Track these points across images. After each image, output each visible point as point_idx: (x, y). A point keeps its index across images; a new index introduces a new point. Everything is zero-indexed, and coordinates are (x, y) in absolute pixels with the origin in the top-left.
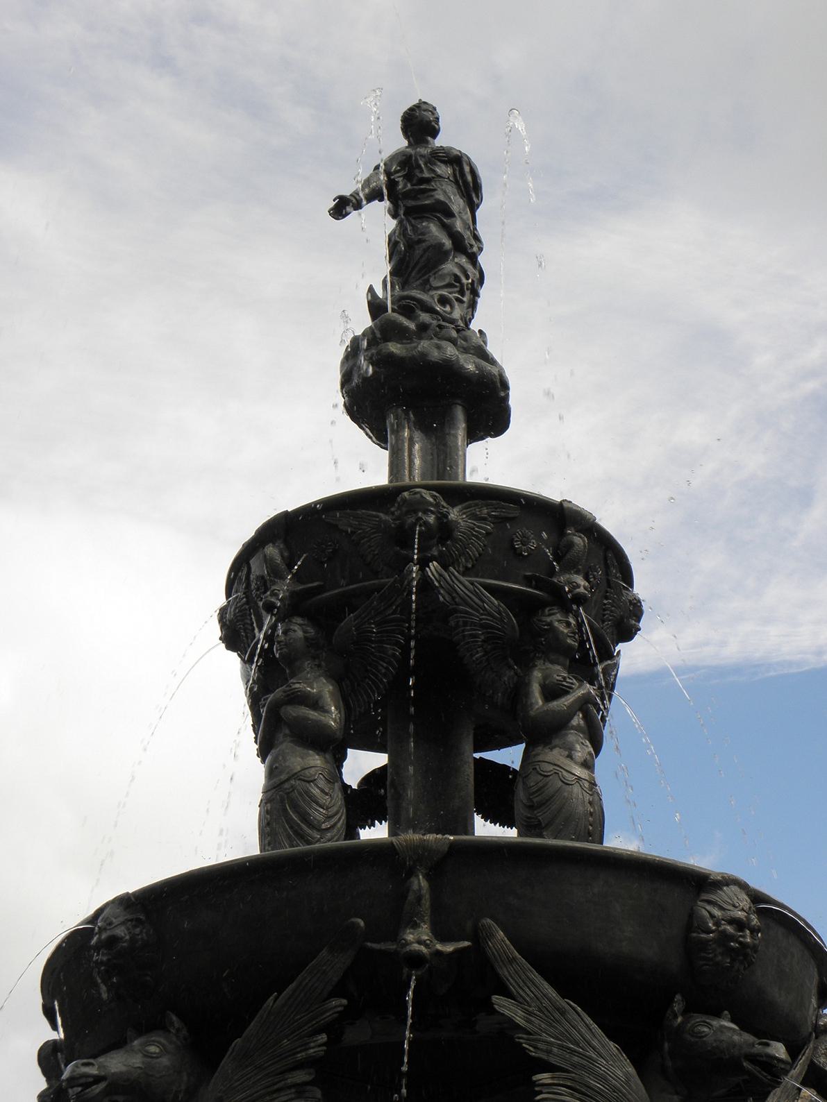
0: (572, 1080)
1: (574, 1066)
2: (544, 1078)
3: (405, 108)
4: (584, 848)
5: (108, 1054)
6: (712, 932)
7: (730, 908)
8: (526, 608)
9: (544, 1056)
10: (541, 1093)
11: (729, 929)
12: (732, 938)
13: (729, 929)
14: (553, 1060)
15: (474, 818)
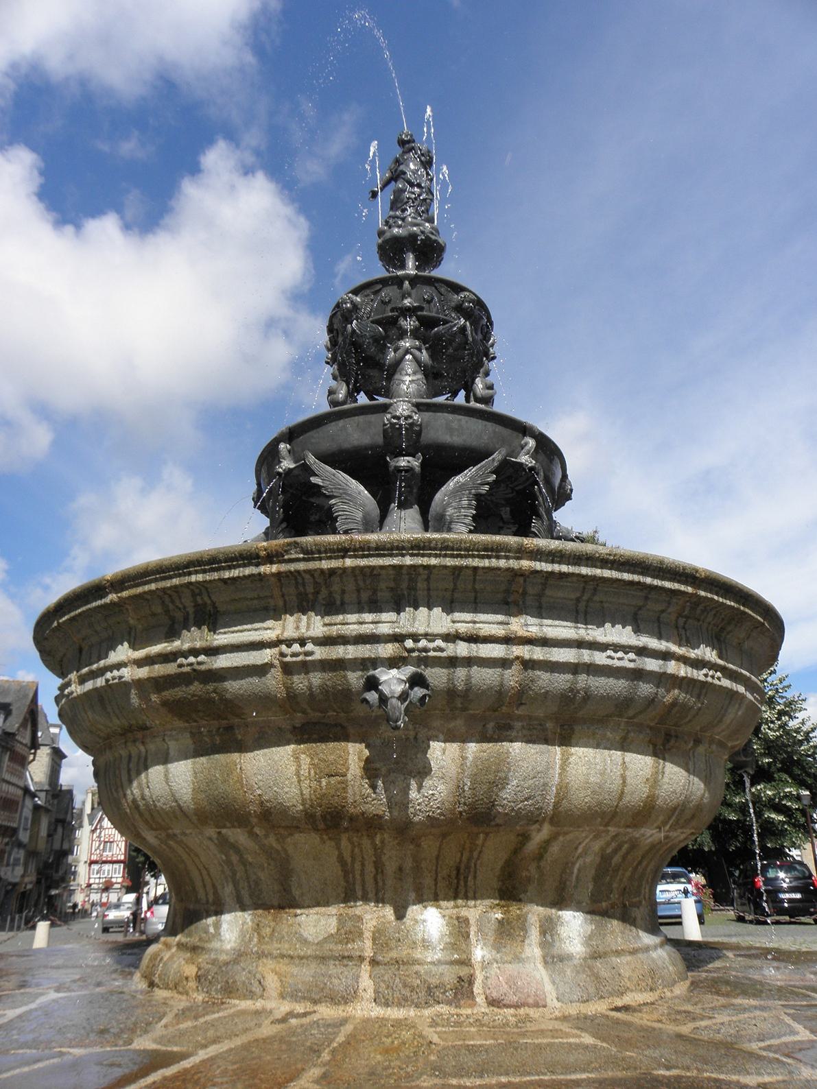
2: (333, 501)
12: (396, 424)
14: (335, 494)
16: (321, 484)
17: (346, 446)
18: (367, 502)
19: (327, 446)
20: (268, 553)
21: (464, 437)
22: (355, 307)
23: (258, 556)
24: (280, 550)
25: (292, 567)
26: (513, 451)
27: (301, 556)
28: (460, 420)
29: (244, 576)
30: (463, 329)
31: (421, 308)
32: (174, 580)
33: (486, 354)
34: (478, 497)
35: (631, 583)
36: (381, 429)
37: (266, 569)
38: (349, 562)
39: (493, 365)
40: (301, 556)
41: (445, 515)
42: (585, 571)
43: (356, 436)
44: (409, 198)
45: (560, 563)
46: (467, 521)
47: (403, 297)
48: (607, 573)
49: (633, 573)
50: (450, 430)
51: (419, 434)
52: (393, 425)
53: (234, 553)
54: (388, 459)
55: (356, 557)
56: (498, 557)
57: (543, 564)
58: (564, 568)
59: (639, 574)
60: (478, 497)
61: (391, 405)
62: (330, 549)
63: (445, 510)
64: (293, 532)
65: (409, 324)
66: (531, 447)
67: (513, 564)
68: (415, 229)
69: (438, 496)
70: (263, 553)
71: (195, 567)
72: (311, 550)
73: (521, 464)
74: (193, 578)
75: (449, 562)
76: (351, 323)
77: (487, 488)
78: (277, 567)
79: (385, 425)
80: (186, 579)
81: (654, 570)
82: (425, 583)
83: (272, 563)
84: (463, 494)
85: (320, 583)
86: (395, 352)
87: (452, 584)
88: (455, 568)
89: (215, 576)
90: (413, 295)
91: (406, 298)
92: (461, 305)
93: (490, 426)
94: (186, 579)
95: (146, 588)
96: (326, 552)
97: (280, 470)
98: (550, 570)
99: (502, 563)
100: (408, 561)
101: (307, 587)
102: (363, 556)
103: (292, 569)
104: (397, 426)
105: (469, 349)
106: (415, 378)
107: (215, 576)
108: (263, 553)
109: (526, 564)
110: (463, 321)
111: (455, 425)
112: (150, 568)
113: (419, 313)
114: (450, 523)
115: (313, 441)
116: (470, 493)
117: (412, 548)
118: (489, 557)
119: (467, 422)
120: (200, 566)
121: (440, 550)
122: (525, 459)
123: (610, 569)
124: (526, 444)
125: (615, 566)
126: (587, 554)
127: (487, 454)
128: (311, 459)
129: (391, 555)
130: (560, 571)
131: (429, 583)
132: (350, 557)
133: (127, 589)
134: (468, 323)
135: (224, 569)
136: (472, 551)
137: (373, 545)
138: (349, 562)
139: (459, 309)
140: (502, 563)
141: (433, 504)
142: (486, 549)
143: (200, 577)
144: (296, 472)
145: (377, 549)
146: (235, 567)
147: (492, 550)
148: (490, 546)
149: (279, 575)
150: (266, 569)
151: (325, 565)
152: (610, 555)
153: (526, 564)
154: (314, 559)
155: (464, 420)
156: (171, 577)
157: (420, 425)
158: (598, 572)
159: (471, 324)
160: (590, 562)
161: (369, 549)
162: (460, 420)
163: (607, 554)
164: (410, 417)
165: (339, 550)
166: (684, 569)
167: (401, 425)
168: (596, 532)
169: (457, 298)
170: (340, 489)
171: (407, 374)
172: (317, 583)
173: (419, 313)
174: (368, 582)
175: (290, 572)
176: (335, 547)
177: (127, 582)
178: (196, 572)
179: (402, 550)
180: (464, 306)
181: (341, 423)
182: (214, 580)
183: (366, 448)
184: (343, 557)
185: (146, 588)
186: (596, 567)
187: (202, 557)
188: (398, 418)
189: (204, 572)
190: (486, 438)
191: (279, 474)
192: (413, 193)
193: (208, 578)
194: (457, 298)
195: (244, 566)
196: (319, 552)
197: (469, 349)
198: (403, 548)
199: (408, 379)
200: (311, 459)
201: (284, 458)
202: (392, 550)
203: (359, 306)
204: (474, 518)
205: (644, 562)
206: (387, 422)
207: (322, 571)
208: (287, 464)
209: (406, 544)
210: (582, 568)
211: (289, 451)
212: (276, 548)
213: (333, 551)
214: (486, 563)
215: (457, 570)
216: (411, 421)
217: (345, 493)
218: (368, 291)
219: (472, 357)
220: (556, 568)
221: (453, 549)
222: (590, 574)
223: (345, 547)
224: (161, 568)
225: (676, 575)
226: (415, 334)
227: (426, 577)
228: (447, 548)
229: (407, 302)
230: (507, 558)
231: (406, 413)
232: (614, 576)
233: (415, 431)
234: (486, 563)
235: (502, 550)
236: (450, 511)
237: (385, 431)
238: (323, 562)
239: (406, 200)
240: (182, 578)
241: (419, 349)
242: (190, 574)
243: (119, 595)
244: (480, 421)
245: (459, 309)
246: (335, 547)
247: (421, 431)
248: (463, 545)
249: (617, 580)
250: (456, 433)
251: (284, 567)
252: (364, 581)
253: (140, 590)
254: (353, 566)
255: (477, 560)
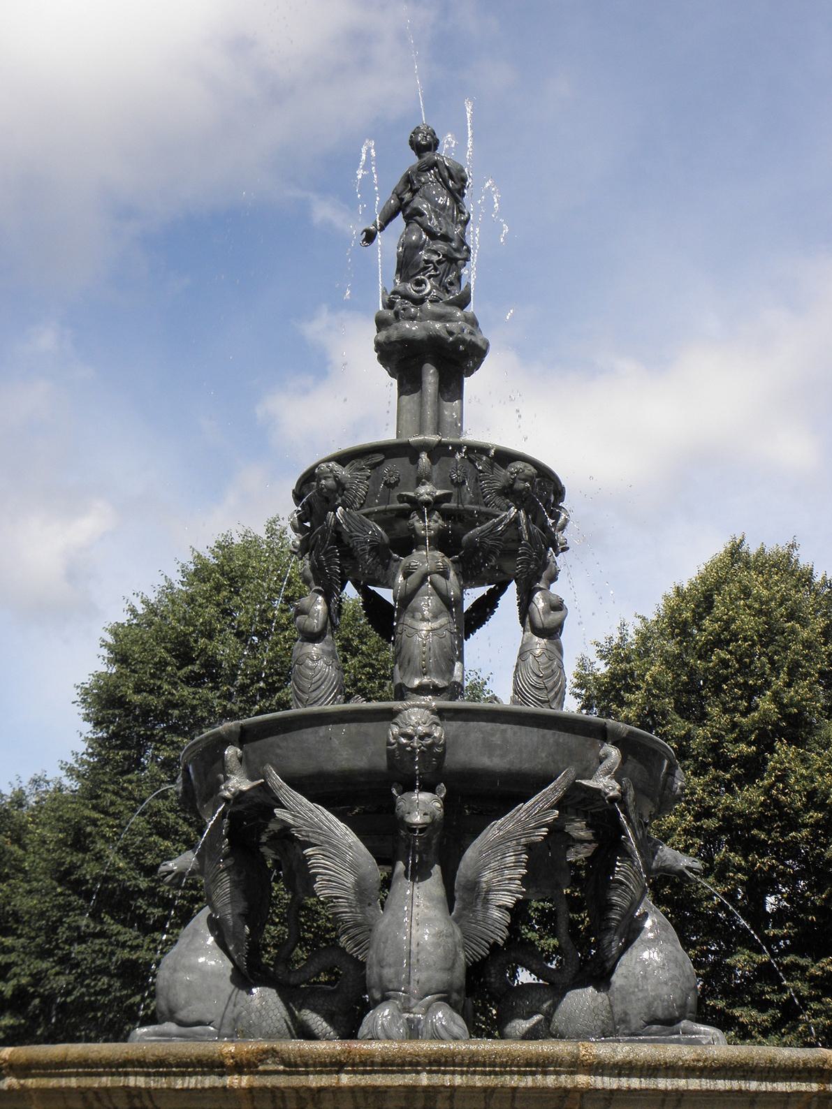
0: (323, 850)
1: (322, 842)
2: (309, 851)
3: (408, 142)
4: (336, 710)
5: (532, 1042)
6: (393, 744)
7: (405, 726)
8: (389, 520)
9: (307, 839)
10: (310, 860)
11: (404, 741)
12: (406, 745)
13: (404, 741)
14: (313, 841)
15: (483, 585)
16: (292, 822)
17: (329, 767)
18: (361, 860)
19: (298, 764)
20: (236, 1062)
21: (511, 757)
22: (340, 486)
23: (222, 1065)
24: (253, 1059)
25: (269, 1081)
26: (586, 769)
27: (281, 1068)
28: (504, 731)
29: (203, 1088)
30: (516, 521)
31: (446, 498)
32: (104, 1079)
33: (552, 543)
34: (530, 848)
35: (730, 1092)
36: (384, 747)
37: (233, 1081)
38: (345, 1080)
39: (561, 560)
40: (281, 1068)
41: (479, 882)
42: (663, 1084)
43: (345, 754)
44: (427, 262)
45: (629, 1076)
46: (513, 887)
47: (419, 481)
48: (694, 1084)
49: (731, 1079)
50: (489, 747)
51: (441, 757)
52: (403, 746)
53: (189, 1057)
54: (394, 792)
55: (354, 1072)
56: (545, 1073)
57: (606, 1079)
58: (635, 1083)
59: (739, 1078)
60: (530, 848)
61: (398, 712)
62: (321, 1062)
63: (479, 874)
64: (218, 765)
65: (427, 525)
66: (614, 764)
67: (565, 1081)
68: (438, 326)
69: (470, 853)
70: (230, 1062)
71: (134, 1067)
72: (296, 1062)
73: (598, 791)
74: (132, 1081)
75: (478, 1081)
76: (335, 511)
77: (544, 831)
78: (249, 1079)
79: (389, 744)
80: (121, 1081)
81: (761, 1071)
82: (448, 1102)
83: (241, 1073)
84: (509, 847)
85: (305, 1099)
86: (405, 578)
87: (483, 1103)
88: (485, 1090)
89: (163, 1083)
90: (434, 475)
91: (424, 484)
92: (512, 485)
93: (550, 735)
94: (121, 1081)
95: (63, 1082)
96: (314, 1065)
97: (227, 794)
98: (615, 1086)
99: (550, 1081)
100: (424, 1080)
101: (288, 1103)
102: (364, 1073)
103: (269, 1085)
104: (409, 749)
105: (523, 554)
106: (435, 625)
107: (163, 1083)
108: (230, 1062)
109: (582, 1080)
110: (513, 511)
111: (497, 740)
112: (68, 1059)
113: (445, 505)
114: (488, 892)
115: (279, 751)
116: (518, 844)
117: (430, 1064)
118: (533, 1073)
119: (515, 733)
120: (142, 1067)
121: (468, 1066)
122: (604, 783)
123: (699, 1077)
124: (606, 756)
125: (705, 1073)
126: (666, 1063)
127: (544, 780)
128: (276, 780)
129: (402, 1072)
130: (629, 1088)
131: (452, 1101)
132: (347, 1072)
133: (33, 1076)
134: (522, 513)
135: (175, 1074)
136: (510, 1066)
137: (378, 1060)
138: (345, 1080)
139: (509, 492)
140: (550, 1081)
141: (462, 865)
142: (528, 1064)
143: (141, 1082)
144: (252, 794)
145: (383, 1064)
146: (191, 1075)
147: (537, 1065)
148: (534, 1061)
149: (251, 1090)
150: (233, 1081)
151: (314, 1081)
152: (698, 1061)
153: (582, 1080)
154: (299, 1073)
155: (510, 730)
156: (99, 1075)
157: (444, 745)
158: (682, 1083)
159: (527, 514)
160: (670, 1072)
161: (373, 1064)
162: (504, 731)
163: (693, 1060)
164: (428, 735)
165: (332, 1064)
166: (805, 1064)
167: (414, 749)
168: (793, 546)
169: (503, 475)
170: (320, 834)
171: (424, 619)
172: (301, 1097)
173: (445, 505)
174: (370, 1101)
175: (266, 1087)
176: (328, 1060)
177: (36, 1068)
178: (136, 1074)
179: (417, 1066)
180: (516, 486)
181: (322, 731)
182: (162, 1088)
183: (361, 773)
184: (338, 1072)
185: (63, 1082)
186: (679, 1077)
187: (144, 1057)
188: (410, 737)
189: (148, 1075)
190: (544, 755)
191: (226, 800)
192: (435, 252)
193: (152, 1084)
194: (503, 475)
195: (203, 1074)
196: (306, 1065)
197: (523, 554)
198: (418, 1064)
199: (425, 627)
200: (276, 780)
201: (232, 773)
202: (403, 1065)
203: (347, 486)
204: (525, 880)
205: (747, 1064)
206: (393, 741)
207: (309, 1089)
208: (238, 783)
209: (422, 1060)
210: (660, 1080)
211: (240, 760)
212: (249, 1056)
213: (324, 1065)
214: (529, 1081)
215: (488, 1092)
216: (429, 741)
217: (328, 843)
218: (362, 463)
219: (529, 564)
220: (625, 1083)
221: (484, 1065)
222: (670, 1088)
223: (341, 1061)
224: (86, 1061)
225: (793, 1072)
226: (443, 542)
227: (448, 1094)
228: (476, 1064)
229: (426, 491)
230: (558, 1073)
231: (422, 729)
232: (704, 1087)
233: (434, 753)
234: (529, 1081)
235: (550, 1064)
236: (487, 876)
237: (390, 754)
238: (311, 1077)
239: (422, 265)
240: (116, 1078)
241: (445, 574)
242: (126, 1074)
243: (22, 1081)
244: (536, 729)
245: (509, 492)
246: (328, 1060)
247: (444, 753)
248: (498, 1060)
249: (709, 1093)
250: (498, 752)
251: (258, 1081)
252: (366, 1099)
253: (53, 1083)
254: (352, 1085)
255: (516, 1077)
